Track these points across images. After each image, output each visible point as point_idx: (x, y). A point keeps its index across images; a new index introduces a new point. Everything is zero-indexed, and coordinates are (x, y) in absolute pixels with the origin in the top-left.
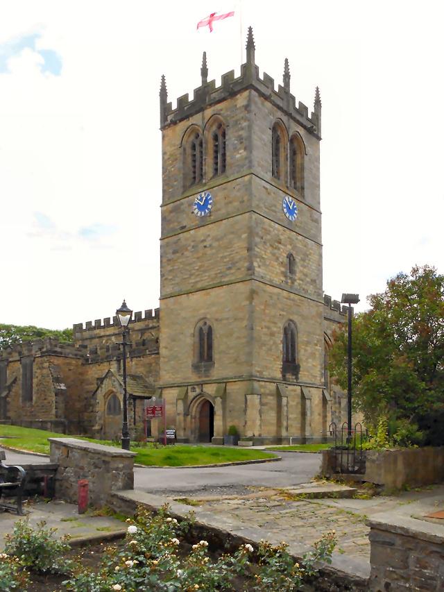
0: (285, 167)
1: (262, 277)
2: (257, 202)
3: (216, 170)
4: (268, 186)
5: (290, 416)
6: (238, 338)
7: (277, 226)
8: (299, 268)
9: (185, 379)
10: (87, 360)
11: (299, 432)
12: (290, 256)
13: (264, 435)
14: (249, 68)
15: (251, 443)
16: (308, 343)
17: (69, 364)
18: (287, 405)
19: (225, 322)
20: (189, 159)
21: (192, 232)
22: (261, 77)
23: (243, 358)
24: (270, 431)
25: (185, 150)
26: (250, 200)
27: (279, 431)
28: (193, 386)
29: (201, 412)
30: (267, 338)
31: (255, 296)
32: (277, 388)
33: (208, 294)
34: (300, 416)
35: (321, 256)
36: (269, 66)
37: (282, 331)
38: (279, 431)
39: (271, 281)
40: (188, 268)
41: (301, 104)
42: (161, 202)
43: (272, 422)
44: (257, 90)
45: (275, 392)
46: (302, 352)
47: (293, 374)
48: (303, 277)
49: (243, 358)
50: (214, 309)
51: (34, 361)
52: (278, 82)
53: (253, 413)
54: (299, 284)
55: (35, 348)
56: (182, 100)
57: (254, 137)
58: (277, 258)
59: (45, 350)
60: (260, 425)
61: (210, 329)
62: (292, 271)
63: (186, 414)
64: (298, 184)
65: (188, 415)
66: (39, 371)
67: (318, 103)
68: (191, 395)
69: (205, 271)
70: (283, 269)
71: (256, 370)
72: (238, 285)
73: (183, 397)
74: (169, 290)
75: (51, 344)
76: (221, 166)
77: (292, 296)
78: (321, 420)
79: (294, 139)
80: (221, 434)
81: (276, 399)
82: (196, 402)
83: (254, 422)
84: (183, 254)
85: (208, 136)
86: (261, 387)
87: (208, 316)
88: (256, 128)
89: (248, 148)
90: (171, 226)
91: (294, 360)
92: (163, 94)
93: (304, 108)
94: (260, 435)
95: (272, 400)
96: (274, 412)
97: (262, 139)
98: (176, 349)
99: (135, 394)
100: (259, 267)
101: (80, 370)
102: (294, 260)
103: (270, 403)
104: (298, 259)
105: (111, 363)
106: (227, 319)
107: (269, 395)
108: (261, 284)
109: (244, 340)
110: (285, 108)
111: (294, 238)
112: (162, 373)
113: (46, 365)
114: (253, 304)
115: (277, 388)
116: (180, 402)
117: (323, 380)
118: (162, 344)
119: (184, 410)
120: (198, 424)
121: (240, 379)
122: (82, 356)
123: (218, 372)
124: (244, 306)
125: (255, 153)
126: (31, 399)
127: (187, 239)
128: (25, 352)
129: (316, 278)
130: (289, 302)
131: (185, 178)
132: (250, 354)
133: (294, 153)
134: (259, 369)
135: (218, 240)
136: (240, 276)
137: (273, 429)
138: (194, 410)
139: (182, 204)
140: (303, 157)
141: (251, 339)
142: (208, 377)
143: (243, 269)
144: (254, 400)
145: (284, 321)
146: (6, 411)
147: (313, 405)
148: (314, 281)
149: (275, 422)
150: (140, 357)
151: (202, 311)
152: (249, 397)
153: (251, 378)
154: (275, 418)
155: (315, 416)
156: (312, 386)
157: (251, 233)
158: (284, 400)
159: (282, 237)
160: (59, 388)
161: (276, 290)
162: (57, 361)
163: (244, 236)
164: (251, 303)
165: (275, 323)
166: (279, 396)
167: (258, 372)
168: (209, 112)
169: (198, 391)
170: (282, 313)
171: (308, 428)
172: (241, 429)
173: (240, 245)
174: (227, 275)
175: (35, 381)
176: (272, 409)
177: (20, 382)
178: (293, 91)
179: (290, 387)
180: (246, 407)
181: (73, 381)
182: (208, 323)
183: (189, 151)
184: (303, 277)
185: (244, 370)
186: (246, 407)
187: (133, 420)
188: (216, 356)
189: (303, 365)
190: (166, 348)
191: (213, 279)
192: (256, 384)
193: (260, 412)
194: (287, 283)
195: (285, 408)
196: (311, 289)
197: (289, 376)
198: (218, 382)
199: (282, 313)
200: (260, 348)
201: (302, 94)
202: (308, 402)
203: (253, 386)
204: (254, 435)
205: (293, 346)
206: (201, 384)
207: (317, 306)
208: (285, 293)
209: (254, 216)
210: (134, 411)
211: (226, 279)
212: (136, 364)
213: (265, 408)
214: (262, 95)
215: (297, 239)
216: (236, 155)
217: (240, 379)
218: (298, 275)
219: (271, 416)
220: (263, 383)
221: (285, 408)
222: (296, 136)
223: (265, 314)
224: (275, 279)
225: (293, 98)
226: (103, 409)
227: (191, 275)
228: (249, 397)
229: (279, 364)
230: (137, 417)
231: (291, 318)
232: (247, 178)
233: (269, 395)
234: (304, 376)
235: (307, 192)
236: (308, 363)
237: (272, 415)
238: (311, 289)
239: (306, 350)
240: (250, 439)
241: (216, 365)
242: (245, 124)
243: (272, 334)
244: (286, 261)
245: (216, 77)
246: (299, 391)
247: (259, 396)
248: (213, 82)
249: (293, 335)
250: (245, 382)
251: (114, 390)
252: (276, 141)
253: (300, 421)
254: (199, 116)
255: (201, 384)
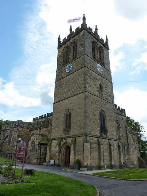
0: (97, 55)
1: (90, 91)
2: (87, 64)
3: (74, 57)
4: (91, 59)
5: (105, 154)
6: (81, 117)
7: (95, 73)
8: (104, 90)
9: (61, 136)
10: (31, 129)
11: (109, 162)
12: (100, 85)
13: (93, 164)
14: (84, 25)
15: (86, 169)
16: (110, 120)
17: (25, 130)
18: (103, 149)
19: (76, 110)
20: (66, 56)
21: (65, 78)
22: (88, 27)
23: (82, 126)
24: (95, 163)
25: (64, 53)
26: (84, 63)
27: (100, 162)
28: (62, 139)
29: (66, 152)
30: (93, 117)
31: (87, 98)
32: (98, 140)
33: (69, 100)
34: (109, 154)
35: (112, 87)
36: (90, 24)
37: (99, 114)
38: (100, 162)
39: (93, 93)
40: (63, 91)
41: (101, 38)
42: (56, 71)
43: (96, 157)
44: (86, 30)
45: (97, 142)
46: (108, 124)
47: (105, 134)
48: (106, 94)
49: (82, 126)
50: (72, 105)
51: (13, 129)
52: (94, 30)
53: (87, 153)
54: (105, 96)
55: (14, 125)
56: (64, 40)
57: (86, 43)
58: (96, 85)
59: (16, 125)
60: (91, 159)
61: (70, 114)
62: (102, 91)
63: (60, 152)
64: (102, 62)
65: (60, 153)
66: (14, 133)
67: (107, 39)
68: (62, 143)
69: (69, 91)
70: (98, 90)
71: (88, 131)
72: (81, 94)
73: (58, 144)
74: (56, 100)
75: (18, 123)
76: (75, 56)
77: (102, 100)
78: (118, 156)
79: (100, 47)
80: (73, 163)
81: (97, 145)
82: (64, 147)
83: (87, 157)
84: (62, 86)
85: (72, 47)
86: (91, 139)
87: (69, 109)
88: (86, 41)
89: (84, 47)
90: (59, 77)
91: (105, 127)
92: (59, 39)
93: (102, 40)
94: (90, 165)
95: (95, 146)
96: (97, 152)
97: (89, 49)
98: (58, 123)
99: (41, 142)
100: (88, 87)
101: (28, 133)
102: (102, 87)
103: (95, 147)
104: (104, 87)
105: (38, 130)
106: (76, 109)
107: (94, 143)
108: (89, 94)
109: (83, 117)
110: (96, 37)
111: (102, 79)
112: (52, 133)
113: (16, 130)
114: (86, 101)
115: (98, 140)
116: (58, 146)
117: (117, 137)
118: (53, 121)
119: (59, 150)
120: (64, 158)
121: (81, 135)
122: (30, 128)
123: (72, 132)
124: (83, 103)
125: (86, 48)
126: (10, 144)
127: (63, 81)
128: (12, 126)
129: (111, 94)
130: (101, 103)
131: (64, 62)
132: (85, 123)
133: (100, 53)
134: (89, 131)
135: (73, 79)
136: (81, 91)
137: (97, 161)
138: (63, 150)
139: (62, 69)
140: (103, 54)
141: (86, 117)
142: (69, 134)
143: (82, 88)
144: (87, 145)
145: (99, 110)
146: (2, 148)
147: (115, 149)
148: (110, 96)
149: (98, 157)
150: (46, 127)
151: (68, 107)
152: (85, 144)
153: (86, 135)
154: (98, 155)
155: (115, 154)
156: (113, 139)
157: (85, 74)
158: (101, 146)
159: (97, 78)
160: (18, 140)
161: (96, 97)
162: (20, 129)
163: (82, 76)
164: (85, 101)
165: (95, 110)
166: (99, 144)
167: (89, 132)
168: (71, 40)
169: (64, 141)
170: (98, 107)
171: (113, 160)
172: (82, 161)
173: (81, 80)
174: (76, 91)
175: (12, 137)
176: (96, 150)
177: (8, 137)
178: (98, 34)
179: (104, 140)
180: (84, 149)
181: (25, 137)
182: (70, 111)
183: (66, 53)
184: (106, 94)
185: (83, 131)
186: (84, 149)
187: (39, 154)
188: (72, 125)
189: (109, 130)
190: (54, 122)
191: (71, 94)
192: (88, 138)
193: (90, 152)
194: (100, 95)
195: (102, 150)
196: (109, 99)
197: (103, 135)
198: (73, 137)
199: (98, 107)
200: (90, 121)
201: (102, 35)
202: (112, 147)
203: (87, 139)
204: (88, 165)
205: (104, 121)
206: (66, 138)
207: (113, 105)
208: (100, 99)
209: (86, 68)
210: (40, 150)
211: (76, 93)
212: (45, 130)
213: (93, 150)
214: (88, 32)
215: (103, 79)
216: (80, 50)
217: (81, 135)
218: (104, 93)
219: (96, 154)
220: (91, 138)
221: (102, 150)
222: (100, 48)
223: (91, 106)
224: (95, 93)
225: (99, 36)
226: (30, 149)
227: (64, 93)
228: (85, 144)
229: (98, 129)
230: (41, 153)
231: (102, 109)
232: (83, 56)
233: (94, 143)
234: (109, 135)
235: (105, 64)
236: (111, 129)
237: (96, 153)
238: (109, 99)
239: (109, 123)
240: (85, 167)
241: (72, 129)
242: (82, 40)
243: (95, 115)
244: (99, 86)
245: (74, 30)
246: (108, 142)
247: (90, 144)
248: (73, 31)
249: (103, 116)
250: (84, 137)
251: (34, 140)
252: (94, 48)
253: (109, 157)
254: (69, 42)
255: (66, 138)
